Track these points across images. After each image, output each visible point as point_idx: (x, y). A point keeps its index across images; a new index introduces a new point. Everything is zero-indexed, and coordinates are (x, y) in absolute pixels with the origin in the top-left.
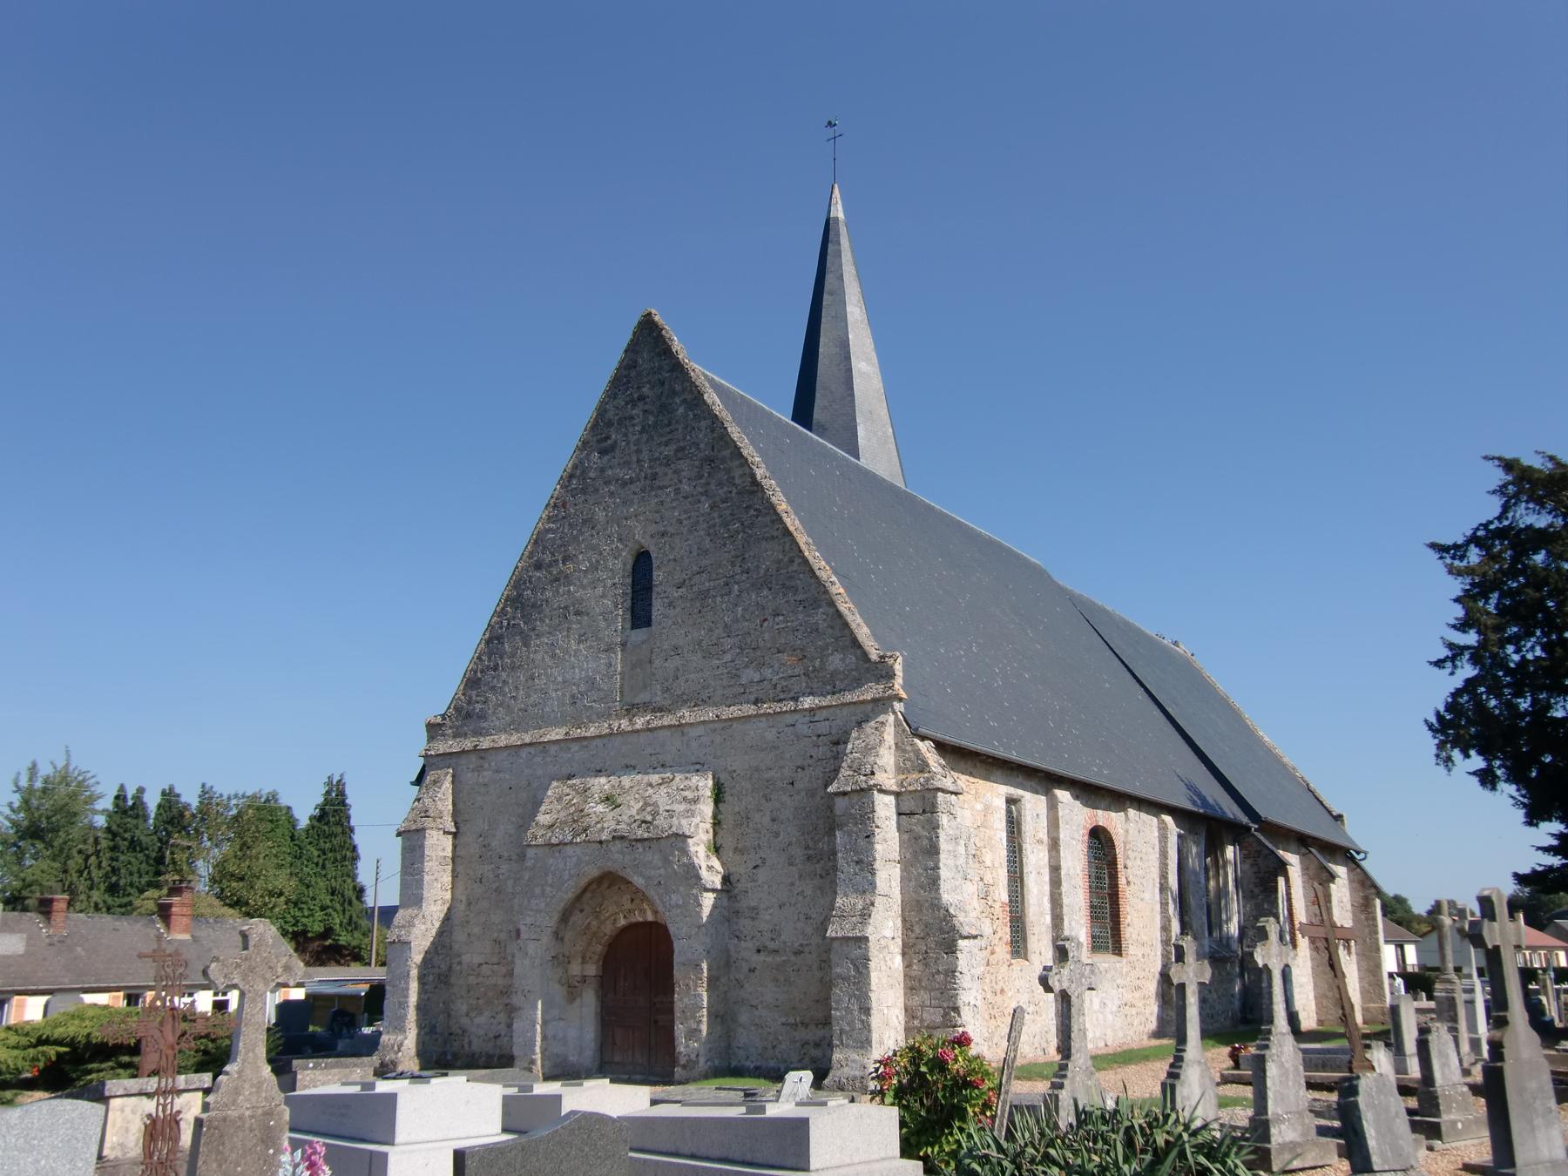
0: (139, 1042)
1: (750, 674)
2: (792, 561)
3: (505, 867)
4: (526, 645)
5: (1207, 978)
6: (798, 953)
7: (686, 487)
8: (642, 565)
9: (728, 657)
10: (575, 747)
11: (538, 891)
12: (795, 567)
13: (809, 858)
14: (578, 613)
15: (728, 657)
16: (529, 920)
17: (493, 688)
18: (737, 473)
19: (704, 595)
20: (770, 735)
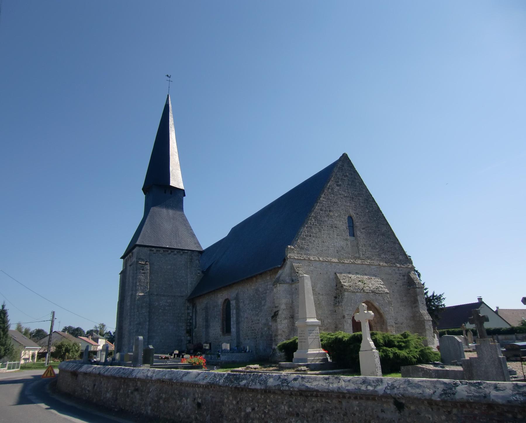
0: (480, 299)
1: (383, 256)
2: (389, 231)
3: (321, 297)
4: (320, 231)
5: (509, 368)
6: (402, 324)
7: (362, 204)
8: (350, 218)
9: (378, 250)
10: (340, 265)
11: (349, 305)
12: (389, 233)
13: (401, 302)
14: (336, 227)
15: (378, 250)
16: (347, 313)
17: (310, 242)
18: (374, 206)
19: (370, 233)
20: (390, 271)
